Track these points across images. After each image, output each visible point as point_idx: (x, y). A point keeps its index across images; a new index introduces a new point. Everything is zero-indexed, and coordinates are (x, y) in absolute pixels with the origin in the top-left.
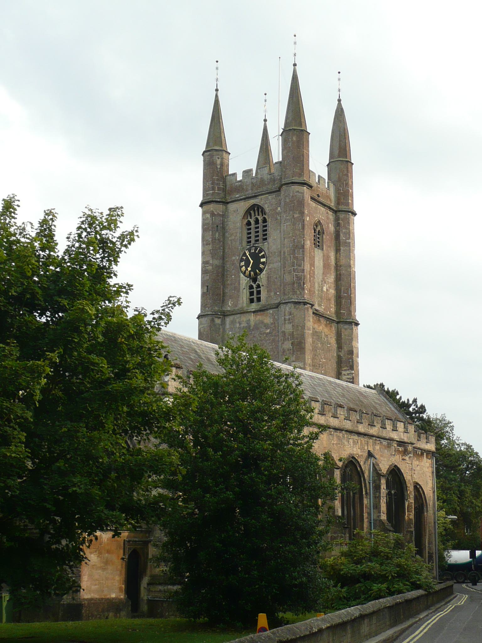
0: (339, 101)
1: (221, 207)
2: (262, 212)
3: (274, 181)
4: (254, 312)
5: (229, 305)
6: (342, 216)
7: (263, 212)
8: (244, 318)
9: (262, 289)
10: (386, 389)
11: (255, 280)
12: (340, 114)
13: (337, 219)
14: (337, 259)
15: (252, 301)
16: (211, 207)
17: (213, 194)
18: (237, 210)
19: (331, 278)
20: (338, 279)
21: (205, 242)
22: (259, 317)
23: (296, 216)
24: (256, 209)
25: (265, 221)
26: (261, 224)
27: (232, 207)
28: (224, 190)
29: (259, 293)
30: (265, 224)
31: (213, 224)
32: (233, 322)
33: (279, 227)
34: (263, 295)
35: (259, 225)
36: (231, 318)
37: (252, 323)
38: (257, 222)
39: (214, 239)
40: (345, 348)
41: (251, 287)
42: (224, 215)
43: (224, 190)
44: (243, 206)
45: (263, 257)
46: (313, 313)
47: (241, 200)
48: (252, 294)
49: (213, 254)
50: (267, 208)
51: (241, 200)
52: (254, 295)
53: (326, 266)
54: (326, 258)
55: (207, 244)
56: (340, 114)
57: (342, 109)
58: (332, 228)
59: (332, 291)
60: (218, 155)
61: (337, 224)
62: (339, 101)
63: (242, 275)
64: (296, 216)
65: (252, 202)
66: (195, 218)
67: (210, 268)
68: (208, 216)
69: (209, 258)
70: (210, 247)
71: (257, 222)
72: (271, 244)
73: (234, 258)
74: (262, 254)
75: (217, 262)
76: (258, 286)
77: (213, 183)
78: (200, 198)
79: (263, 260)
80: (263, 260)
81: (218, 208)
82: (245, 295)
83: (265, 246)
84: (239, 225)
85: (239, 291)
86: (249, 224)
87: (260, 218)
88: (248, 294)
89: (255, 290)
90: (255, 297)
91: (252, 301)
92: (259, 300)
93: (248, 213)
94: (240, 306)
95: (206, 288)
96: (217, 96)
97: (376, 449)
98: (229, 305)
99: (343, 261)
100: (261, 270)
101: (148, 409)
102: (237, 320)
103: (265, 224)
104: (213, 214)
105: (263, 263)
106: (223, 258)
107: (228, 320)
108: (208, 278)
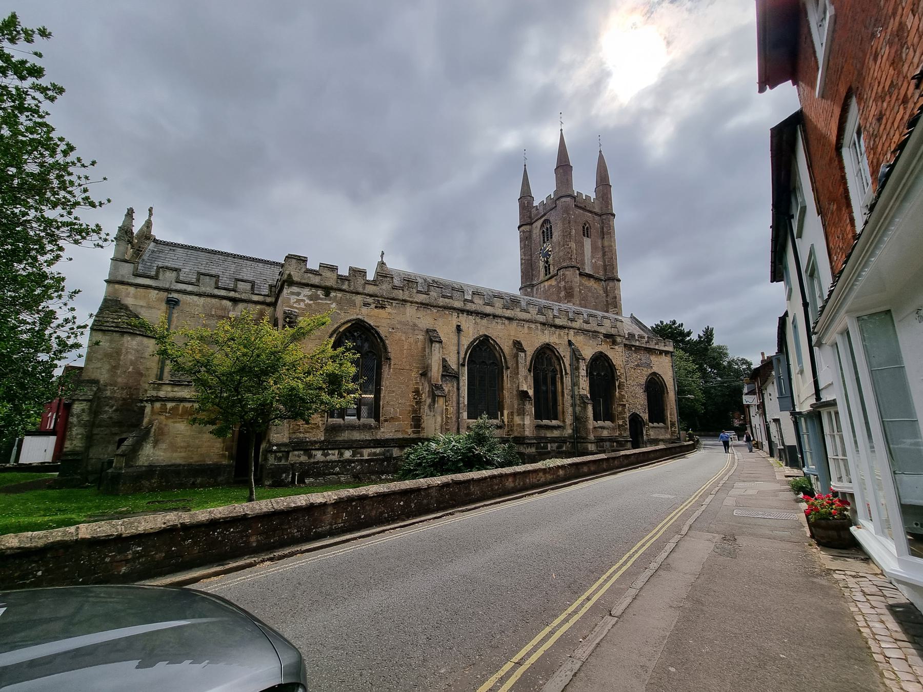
6: (604, 217)
40: (611, 295)
46: (580, 274)
97: (579, 341)
99: (606, 244)
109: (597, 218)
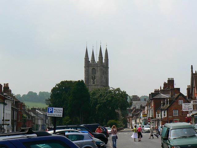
1: (88, 68)
5: (89, 84)
12: (106, 50)
13: (106, 69)
15: (93, 84)
16: (86, 68)
18: (91, 69)
19: (105, 79)
20: (106, 79)
22: (95, 87)
32: (90, 87)
44: (92, 68)
49: (87, 75)
52: (94, 83)
54: (104, 76)
56: (106, 50)
61: (106, 70)
66: (83, 70)
81: (87, 68)
91: (93, 84)
93: (93, 69)
98: (89, 84)
101: (136, 121)
106: (88, 76)
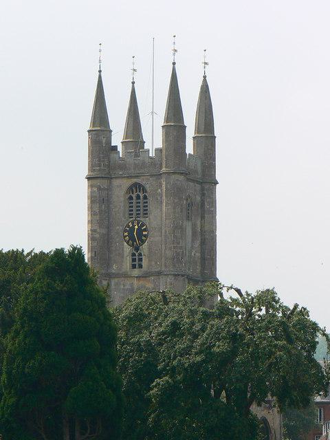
0: (205, 77)
1: (106, 181)
2: (143, 189)
3: (155, 165)
4: (137, 277)
6: (207, 187)
7: (144, 190)
8: (128, 282)
9: (143, 257)
10: (230, 300)
11: (137, 249)
12: (205, 91)
14: (202, 227)
15: (134, 267)
16: (98, 182)
17: (100, 170)
18: (120, 187)
20: (203, 243)
21: (91, 208)
23: (176, 201)
24: (138, 186)
25: (145, 197)
26: (141, 200)
27: (116, 182)
28: (109, 166)
29: (141, 260)
30: (145, 201)
31: (100, 197)
32: (117, 284)
33: (160, 207)
34: (145, 263)
35: (141, 201)
36: (116, 280)
37: (135, 286)
38: (138, 197)
39: (101, 212)
41: (134, 255)
42: (109, 189)
43: (109, 166)
44: (127, 183)
45: (145, 230)
47: (124, 177)
48: (134, 260)
49: (100, 223)
50: (147, 187)
51: (124, 177)
52: (136, 262)
53: (194, 233)
54: (194, 226)
55: (94, 215)
57: (207, 86)
58: (198, 198)
59: (198, 255)
60: (104, 134)
62: (205, 77)
63: (125, 244)
64: (176, 201)
65: (135, 180)
66: (82, 191)
67: (97, 236)
68: (95, 189)
69: (96, 227)
70: (98, 217)
71: (138, 197)
72: (152, 220)
73: (118, 228)
74: (144, 227)
75: (104, 231)
76: (140, 254)
77: (99, 161)
78: (86, 172)
79: (144, 233)
80: (144, 233)
81: (104, 183)
82: (128, 262)
83: (146, 221)
84: (122, 199)
85: (123, 257)
86: (131, 198)
87: (142, 195)
88: (131, 260)
89: (137, 258)
90: (137, 263)
91: (134, 267)
92: (141, 266)
93: (130, 189)
94: (123, 270)
95: (94, 253)
96: (100, 77)
99: (207, 228)
100: (143, 242)
102: (122, 283)
103: (145, 201)
104: (99, 189)
105: (145, 236)
107: (113, 282)
108: (96, 244)
109: (198, 187)
